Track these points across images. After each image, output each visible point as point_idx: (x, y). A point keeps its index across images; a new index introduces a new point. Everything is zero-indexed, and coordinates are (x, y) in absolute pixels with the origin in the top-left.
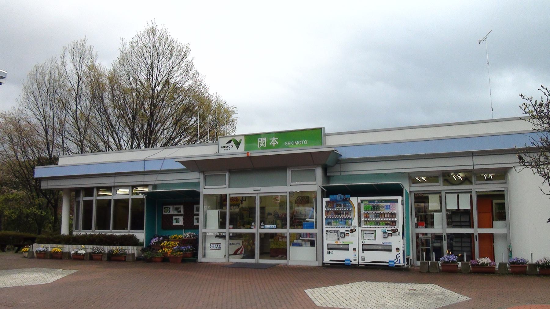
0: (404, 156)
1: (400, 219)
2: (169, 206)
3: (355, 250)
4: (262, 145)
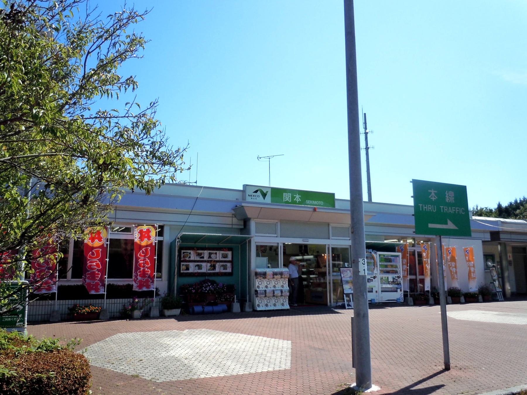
0: (444, 343)
1: (400, 269)
2: (189, 251)
3: (376, 292)
4: (287, 199)
